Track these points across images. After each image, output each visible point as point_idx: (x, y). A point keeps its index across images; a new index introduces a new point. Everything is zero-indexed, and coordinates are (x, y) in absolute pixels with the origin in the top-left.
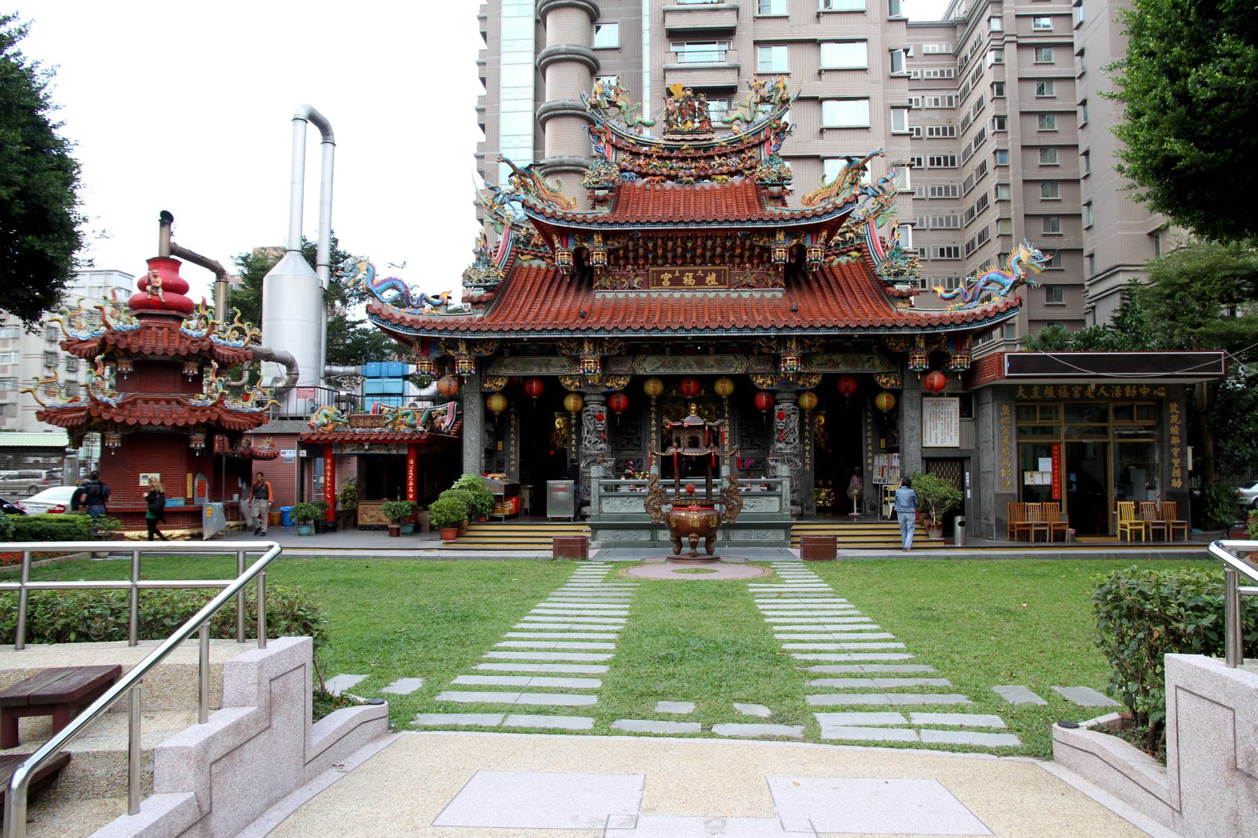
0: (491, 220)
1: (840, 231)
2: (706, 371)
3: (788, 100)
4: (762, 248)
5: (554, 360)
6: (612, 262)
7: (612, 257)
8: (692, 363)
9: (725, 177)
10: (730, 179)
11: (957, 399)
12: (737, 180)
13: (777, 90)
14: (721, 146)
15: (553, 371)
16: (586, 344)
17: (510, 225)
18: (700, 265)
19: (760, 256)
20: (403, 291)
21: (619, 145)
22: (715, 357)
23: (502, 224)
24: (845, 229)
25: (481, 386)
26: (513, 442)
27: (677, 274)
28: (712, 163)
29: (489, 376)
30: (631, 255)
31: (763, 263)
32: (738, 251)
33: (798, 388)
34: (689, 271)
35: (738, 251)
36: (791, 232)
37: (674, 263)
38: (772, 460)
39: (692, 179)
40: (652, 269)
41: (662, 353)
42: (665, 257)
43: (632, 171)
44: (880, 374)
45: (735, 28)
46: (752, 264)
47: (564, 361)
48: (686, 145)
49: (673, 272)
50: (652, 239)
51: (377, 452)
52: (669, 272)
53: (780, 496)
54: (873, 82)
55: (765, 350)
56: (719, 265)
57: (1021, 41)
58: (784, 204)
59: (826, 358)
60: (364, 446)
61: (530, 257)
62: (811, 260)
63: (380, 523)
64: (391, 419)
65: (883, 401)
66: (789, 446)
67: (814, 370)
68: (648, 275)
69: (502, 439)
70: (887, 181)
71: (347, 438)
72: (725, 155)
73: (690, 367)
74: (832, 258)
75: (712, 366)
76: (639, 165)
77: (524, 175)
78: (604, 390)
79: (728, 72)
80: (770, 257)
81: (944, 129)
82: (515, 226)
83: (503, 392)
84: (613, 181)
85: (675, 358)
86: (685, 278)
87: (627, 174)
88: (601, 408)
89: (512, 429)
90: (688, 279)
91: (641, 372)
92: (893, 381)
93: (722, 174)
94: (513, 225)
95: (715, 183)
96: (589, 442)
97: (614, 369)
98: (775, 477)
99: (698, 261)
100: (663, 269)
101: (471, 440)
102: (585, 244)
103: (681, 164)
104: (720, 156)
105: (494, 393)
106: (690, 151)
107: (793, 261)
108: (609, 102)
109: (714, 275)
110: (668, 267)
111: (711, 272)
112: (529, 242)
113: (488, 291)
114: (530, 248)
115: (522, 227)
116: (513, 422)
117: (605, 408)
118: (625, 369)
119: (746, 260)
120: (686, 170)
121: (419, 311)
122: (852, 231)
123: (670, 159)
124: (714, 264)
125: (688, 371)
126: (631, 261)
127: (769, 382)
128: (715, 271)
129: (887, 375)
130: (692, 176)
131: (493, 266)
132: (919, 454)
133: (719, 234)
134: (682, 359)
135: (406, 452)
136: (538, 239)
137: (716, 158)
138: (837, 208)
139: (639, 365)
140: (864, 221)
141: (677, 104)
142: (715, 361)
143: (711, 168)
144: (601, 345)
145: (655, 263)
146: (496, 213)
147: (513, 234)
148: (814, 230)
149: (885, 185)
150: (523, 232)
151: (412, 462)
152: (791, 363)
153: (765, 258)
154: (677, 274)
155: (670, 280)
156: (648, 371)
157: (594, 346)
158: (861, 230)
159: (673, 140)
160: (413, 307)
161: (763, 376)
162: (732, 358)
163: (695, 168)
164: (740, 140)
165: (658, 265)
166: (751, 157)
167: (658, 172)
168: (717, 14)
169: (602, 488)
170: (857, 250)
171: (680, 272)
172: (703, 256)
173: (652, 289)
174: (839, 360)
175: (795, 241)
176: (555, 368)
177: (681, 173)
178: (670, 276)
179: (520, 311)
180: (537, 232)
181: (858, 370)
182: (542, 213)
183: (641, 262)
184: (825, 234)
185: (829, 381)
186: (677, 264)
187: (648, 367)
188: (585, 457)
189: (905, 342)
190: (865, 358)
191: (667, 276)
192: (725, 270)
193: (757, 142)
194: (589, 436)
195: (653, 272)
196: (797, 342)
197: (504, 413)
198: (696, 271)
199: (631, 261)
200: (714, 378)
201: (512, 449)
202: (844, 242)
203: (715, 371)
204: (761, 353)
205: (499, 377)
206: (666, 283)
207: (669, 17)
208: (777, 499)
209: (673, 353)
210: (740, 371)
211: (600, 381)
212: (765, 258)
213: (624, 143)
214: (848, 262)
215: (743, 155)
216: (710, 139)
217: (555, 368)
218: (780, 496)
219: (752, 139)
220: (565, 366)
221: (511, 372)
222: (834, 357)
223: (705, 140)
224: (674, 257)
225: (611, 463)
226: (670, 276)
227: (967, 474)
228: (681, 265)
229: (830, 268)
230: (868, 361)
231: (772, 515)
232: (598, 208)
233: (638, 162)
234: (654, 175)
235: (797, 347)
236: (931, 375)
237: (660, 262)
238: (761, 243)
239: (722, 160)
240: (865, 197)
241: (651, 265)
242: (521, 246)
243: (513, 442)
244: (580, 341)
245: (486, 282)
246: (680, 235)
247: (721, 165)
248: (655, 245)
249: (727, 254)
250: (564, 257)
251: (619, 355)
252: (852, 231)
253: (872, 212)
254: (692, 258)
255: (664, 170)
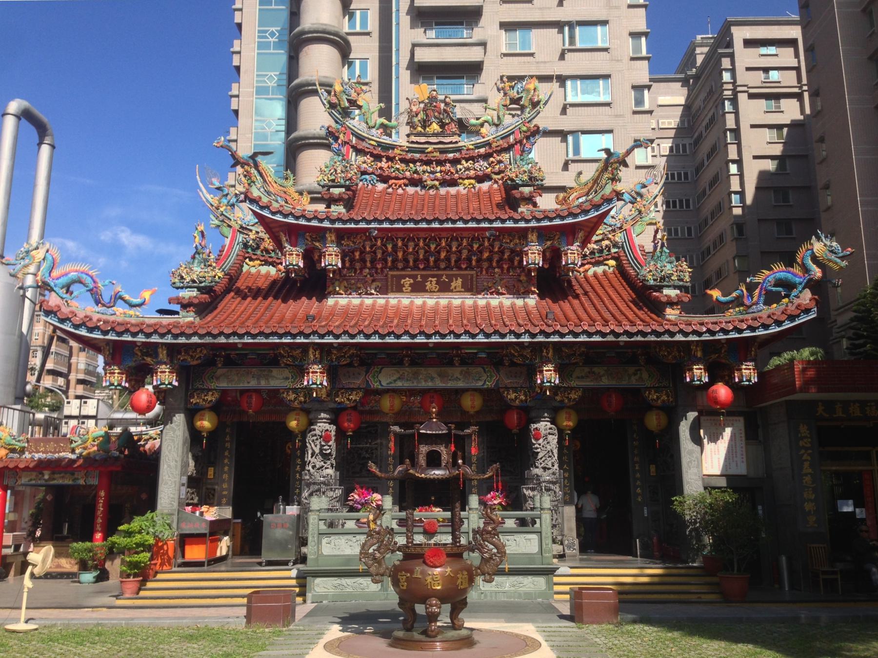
0: (217, 222)
1: (595, 238)
2: (451, 385)
3: (539, 102)
4: (512, 251)
5: (275, 372)
6: (347, 265)
7: (347, 259)
8: (435, 376)
9: (473, 181)
10: (477, 185)
11: (742, 419)
12: (485, 186)
13: (528, 91)
14: (468, 150)
15: (275, 383)
16: (311, 351)
17: (237, 227)
18: (445, 269)
19: (511, 260)
20: (91, 286)
21: (359, 147)
22: (460, 369)
23: (229, 226)
24: (600, 237)
25: (187, 402)
26: (226, 469)
27: (419, 279)
28: (459, 167)
29: (198, 389)
30: (368, 258)
31: (514, 268)
32: (486, 255)
33: (556, 404)
34: (433, 276)
35: (486, 255)
36: (543, 234)
37: (416, 267)
38: (527, 489)
39: (437, 183)
40: (391, 273)
41: (400, 363)
42: (406, 260)
43: (373, 173)
44: (649, 389)
45: (482, 6)
46: (502, 269)
47: (287, 373)
48: (431, 148)
49: (414, 277)
50: (391, 239)
51: (61, 482)
52: (410, 276)
53: (540, 533)
54: (617, 116)
55: (519, 361)
56: (466, 269)
57: (752, 91)
58: (535, 205)
59: (587, 369)
60: (43, 475)
61: (258, 262)
62: (567, 264)
63: (59, 570)
64: (80, 442)
65: (654, 421)
66: (548, 472)
67: (573, 384)
68: (387, 280)
69: (212, 464)
70: (644, 186)
71: (22, 466)
72: (472, 158)
73: (432, 379)
74: (587, 267)
75: (458, 379)
76: (381, 168)
77: (248, 165)
78: (332, 405)
79: (476, 104)
80: (521, 261)
81: (679, 175)
82: (243, 229)
83: (215, 408)
84: (350, 179)
85: (415, 369)
86: (428, 284)
87: (367, 177)
88: (327, 426)
89: (226, 454)
90: (432, 283)
91: (376, 385)
92: (665, 397)
93: (469, 178)
94: (242, 227)
95: (461, 188)
96: (314, 467)
97: (345, 382)
98: (532, 509)
99: (443, 265)
100: (403, 273)
101: (169, 466)
102: (317, 244)
103: (425, 167)
104: (467, 160)
105: (203, 409)
106: (435, 154)
107: (546, 266)
108: (349, 101)
109: (460, 280)
110: (409, 272)
111: (456, 276)
112: (258, 247)
113: (202, 293)
114: (259, 252)
115: (251, 231)
116: (228, 445)
117: (333, 428)
118: (358, 382)
119: (494, 264)
120: (429, 174)
121: (110, 311)
122: (608, 239)
123: (414, 161)
124: (460, 268)
125: (430, 384)
126: (369, 265)
127: (523, 397)
128: (462, 276)
129: (657, 389)
130: (437, 180)
131: (210, 266)
132: (700, 483)
133: (465, 234)
134: (422, 370)
135: (95, 482)
136: (268, 244)
137: (463, 162)
138: (597, 207)
139: (373, 377)
140: (621, 228)
141: (422, 105)
142: (461, 373)
143: (457, 172)
144: (329, 353)
145: (394, 267)
146: (222, 214)
147: (240, 238)
148: (569, 232)
149: (644, 191)
150: (252, 236)
151: (102, 494)
152: (549, 375)
153: (516, 263)
154: (419, 279)
155: (411, 285)
156: (384, 383)
157: (321, 354)
158: (619, 237)
159: (417, 143)
160: (104, 305)
161: (515, 390)
162: (480, 369)
163: (441, 172)
164: (488, 144)
165: (398, 269)
166: (500, 162)
167: (401, 176)
168: (465, 48)
169: (322, 523)
170: (613, 258)
171: (422, 276)
172: (448, 259)
173: (391, 295)
174: (602, 373)
175: (549, 243)
176: (278, 380)
177: (425, 177)
178: (412, 281)
179: (239, 316)
180: (267, 236)
181: (624, 383)
182: (266, 207)
183: (379, 266)
184: (581, 235)
185: (592, 396)
186: (419, 269)
187: (385, 379)
188: (308, 485)
189: (679, 352)
190: (632, 370)
191: (408, 282)
192: (472, 275)
193: (506, 145)
194: (313, 460)
195: (393, 276)
196: (553, 349)
197: (213, 434)
198: (440, 276)
199: (369, 265)
200: (459, 392)
201: (225, 476)
202: (601, 251)
203: (461, 384)
204: (513, 364)
205: (210, 390)
206: (407, 288)
207: (418, 51)
208: (534, 537)
209: (413, 363)
210: (489, 384)
211: (328, 395)
212: (516, 263)
213: (364, 144)
214: (604, 272)
215: (492, 159)
216: (456, 142)
217: (278, 380)
218: (540, 533)
219: (501, 142)
220: (287, 378)
221: (224, 385)
222: (596, 370)
223: (451, 143)
224: (416, 260)
225: (339, 492)
226: (412, 281)
227: (760, 507)
228: (424, 269)
229: (586, 277)
230: (635, 374)
231: (529, 557)
232: (333, 208)
233: (379, 164)
234: (397, 178)
235: (554, 355)
236: (714, 388)
237: (400, 265)
238: (512, 246)
239: (469, 164)
240: (621, 203)
241: (391, 269)
242: (249, 250)
243: (226, 469)
244: (304, 347)
245: (201, 282)
246: (422, 235)
247: (468, 169)
248: (395, 247)
249: (474, 258)
250: (294, 258)
251: (350, 365)
252: (608, 239)
253: (630, 218)
254: (435, 261)
255: (408, 174)
